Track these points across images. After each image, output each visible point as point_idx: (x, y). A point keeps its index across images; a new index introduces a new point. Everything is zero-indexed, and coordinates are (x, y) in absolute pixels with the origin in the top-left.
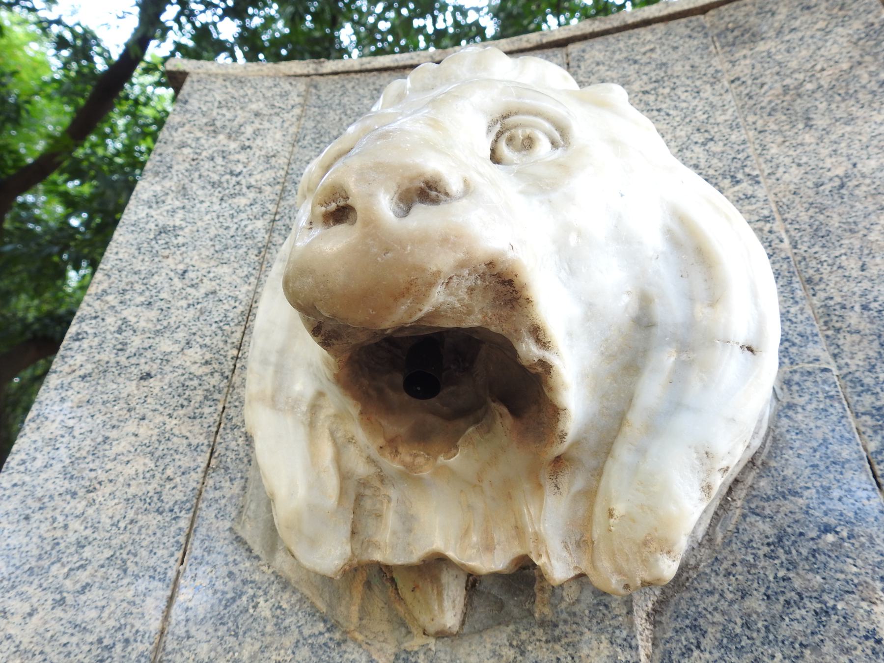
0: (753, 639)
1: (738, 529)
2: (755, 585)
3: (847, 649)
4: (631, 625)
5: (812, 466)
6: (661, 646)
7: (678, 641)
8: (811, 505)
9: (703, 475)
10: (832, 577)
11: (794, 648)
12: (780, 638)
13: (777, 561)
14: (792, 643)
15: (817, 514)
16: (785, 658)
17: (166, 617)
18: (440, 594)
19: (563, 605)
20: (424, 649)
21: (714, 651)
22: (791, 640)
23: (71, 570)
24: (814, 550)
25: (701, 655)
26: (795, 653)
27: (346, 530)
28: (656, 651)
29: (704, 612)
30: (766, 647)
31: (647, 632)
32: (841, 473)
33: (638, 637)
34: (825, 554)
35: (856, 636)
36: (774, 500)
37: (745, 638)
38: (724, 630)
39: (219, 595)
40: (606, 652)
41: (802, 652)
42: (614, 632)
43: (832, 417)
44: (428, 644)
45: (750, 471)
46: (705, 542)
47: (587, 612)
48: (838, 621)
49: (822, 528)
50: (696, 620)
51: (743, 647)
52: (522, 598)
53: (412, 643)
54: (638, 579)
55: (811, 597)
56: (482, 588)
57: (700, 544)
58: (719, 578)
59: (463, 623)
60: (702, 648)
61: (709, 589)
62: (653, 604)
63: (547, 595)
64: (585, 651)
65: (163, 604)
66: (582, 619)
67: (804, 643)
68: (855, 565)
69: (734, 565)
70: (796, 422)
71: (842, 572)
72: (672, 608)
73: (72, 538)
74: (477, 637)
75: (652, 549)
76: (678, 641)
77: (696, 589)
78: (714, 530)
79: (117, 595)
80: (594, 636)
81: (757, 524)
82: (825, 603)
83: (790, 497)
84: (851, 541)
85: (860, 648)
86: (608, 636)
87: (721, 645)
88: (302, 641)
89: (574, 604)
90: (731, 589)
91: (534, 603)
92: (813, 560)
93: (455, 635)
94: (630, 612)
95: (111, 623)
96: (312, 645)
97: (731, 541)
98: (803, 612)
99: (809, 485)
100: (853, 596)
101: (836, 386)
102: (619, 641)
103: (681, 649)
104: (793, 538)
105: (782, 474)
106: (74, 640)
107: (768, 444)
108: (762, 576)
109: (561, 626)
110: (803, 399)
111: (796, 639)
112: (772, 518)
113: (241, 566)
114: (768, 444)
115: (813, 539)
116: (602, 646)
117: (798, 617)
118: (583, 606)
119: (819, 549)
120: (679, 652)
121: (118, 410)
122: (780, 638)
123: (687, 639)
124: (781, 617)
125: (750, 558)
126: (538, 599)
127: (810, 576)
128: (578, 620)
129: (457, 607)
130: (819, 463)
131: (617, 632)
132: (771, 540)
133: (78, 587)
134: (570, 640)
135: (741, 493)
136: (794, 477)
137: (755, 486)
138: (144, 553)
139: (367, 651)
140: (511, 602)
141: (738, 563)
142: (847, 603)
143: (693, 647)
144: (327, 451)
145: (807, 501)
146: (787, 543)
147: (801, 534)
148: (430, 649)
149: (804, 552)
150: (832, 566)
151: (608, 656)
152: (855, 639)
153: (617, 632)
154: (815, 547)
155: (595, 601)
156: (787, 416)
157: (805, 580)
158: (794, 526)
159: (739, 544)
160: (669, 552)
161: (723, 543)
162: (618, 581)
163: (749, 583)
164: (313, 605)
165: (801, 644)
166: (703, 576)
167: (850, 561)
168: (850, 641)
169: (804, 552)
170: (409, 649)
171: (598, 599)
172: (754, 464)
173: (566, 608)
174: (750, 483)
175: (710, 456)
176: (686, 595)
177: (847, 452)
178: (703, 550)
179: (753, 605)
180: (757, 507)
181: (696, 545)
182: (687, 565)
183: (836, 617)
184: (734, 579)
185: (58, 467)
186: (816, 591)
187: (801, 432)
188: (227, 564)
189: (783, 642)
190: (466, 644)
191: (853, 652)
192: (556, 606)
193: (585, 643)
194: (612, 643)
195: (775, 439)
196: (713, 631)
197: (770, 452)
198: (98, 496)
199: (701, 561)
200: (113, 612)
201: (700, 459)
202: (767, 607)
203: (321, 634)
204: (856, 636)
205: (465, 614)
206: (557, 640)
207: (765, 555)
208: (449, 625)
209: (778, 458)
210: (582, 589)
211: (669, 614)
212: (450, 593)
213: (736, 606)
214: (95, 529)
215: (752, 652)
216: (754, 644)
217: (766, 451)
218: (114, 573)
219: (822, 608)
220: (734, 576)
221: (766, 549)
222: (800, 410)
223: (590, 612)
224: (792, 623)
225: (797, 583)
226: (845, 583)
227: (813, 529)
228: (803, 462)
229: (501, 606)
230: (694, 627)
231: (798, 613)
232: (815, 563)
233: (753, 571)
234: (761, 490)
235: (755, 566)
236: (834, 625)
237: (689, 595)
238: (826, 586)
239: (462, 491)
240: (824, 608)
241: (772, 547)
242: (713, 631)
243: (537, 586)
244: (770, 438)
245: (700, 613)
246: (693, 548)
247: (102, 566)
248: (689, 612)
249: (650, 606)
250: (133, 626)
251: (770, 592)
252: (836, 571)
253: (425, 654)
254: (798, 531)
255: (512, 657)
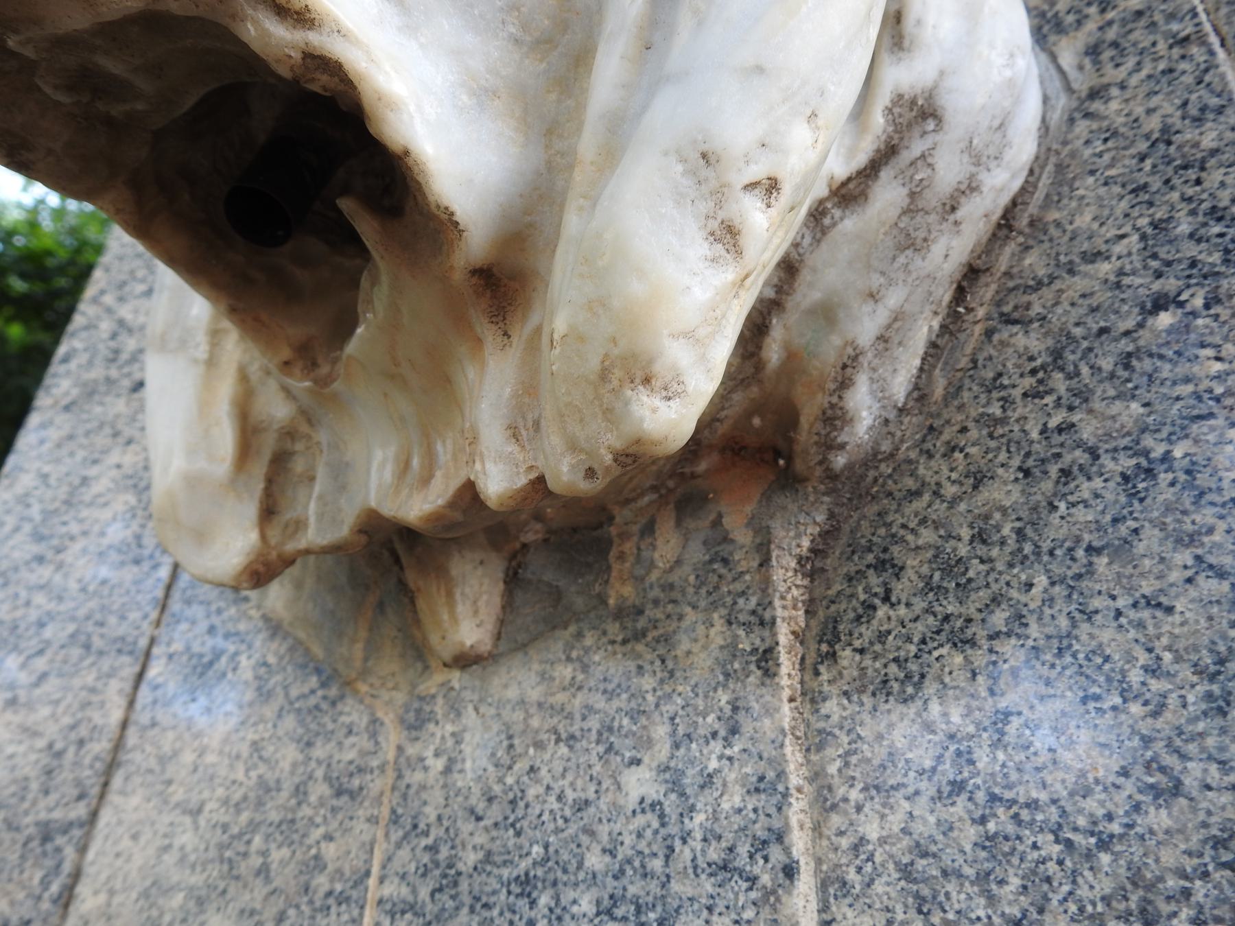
0: (991, 560)
1: (974, 362)
2: (1003, 456)
3: (1191, 536)
4: (766, 585)
5: (1133, 191)
6: (821, 614)
7: (852, 596)
8: (1128, 268)
9: (705, 207)
10: (1166, 397)
11: (1073, 559)
12: (1046, 546)
13: (1049, 400)
14: (1070, 550)
15: (1138, 281)
16: (1053, 584)
17: (131, 703)
18: (450, 594)
19: (654, 576)
20: (444, 690)
21: (915, 600)
22: (1067, 544)
23: (29, 658)
24: (1129, 355)
25: (891, 613)
26: (1076, 569)
27: (250, 509)
28: (813, 623)
29: (902, 532)
30: (1015, 571)
31: (795, 592)
32: (1198, 182)
33: (777, 603)
34: (1151, 355)
35: (1212, 504)
36: (1050, 283)
37: (976, 561)
38: (936, 556)
39: (194, 661)
40: (720, 641)
41: (1091, 564)
42: (735, 603)
43: (1183, 78)
44: (449, 681)
45: (1002, 247)
46: (911, 404)
47: (692, 578)
48: (1172, 484)
49: (1149, 305)
50: (885, 550)
51: (970, 580)
52: (590, 578)
53: (429, 683)
54: (603, 451)
55: (1115, 450)
56: (529, 575)
57: (901, 411)
58: (933, 463)
59: (498, 637)
60: (894, 599)
61: (914, 488)
62: (812, 541)
63: (627, 565)
64: (685, 645)
65: (128, 687)
66: (683, 592)
67: (1096, 544)
68: (1218, 359)
69: (964, 430)
70: (1106, 118)
71: (1187, 380)
72: (844, 540)
73: (33, 615)
74: (520, 655)
75: (615, 383)
76: (852, 596)
77: (890, 494)
78: (930, 376)
79: (77, 682)
80: (701, 617)
81: (1013, 340)
82: (1146, 453)
83: (1084, 268)
84: (1212, 312)
85: (1222, 526)
86: (724, 612)
87: (929, 587)
88: (287, 707)
89: (671, 569)
90: (954, 476)
91: (607, 582)
92: (1126, 374)
93: (486, 659)
94: (765, 562)
95: (67, 720)
96: (299, 711)
97: (960, 388)
98: (1098, 483)
99: (1127, 229)
100: (1212, 422)
101: (1195, 15)
102: (742, 618)
103: (855, 610)
104: (1085, 344)
105: (1070, 228)
106: (21, 749)
107: (1045, 182)
108: (1017, 435)
109: (650, 612)
110: (1122, 68)
111: (1078, 540)
112: (1044, 318)
113: (226, 615)
114: (1045, 182)
115: (1127, 333)
116: (713, 632)
117: (1086, 495)
118: (686, 569)
119: (1138, 349)
120: (852, 615)
121: (101, 440)
122: (1046, 546)
123: (867, 590)
124: (1051, 504)
125: (996, 410)
126: (614, 574)
127: (1117, 406)
128: (676, 595)
129: (483, 611)
130: (1149, 179)
131: (741, 601)
132: (1039, 362)
133: (33, 678)
134: (661, 631)
135: (986, 291)
136: (1095, 226)
137: (1015, 270)
138: (113, 620)
139: (370, 707)
140: (573, 589)
141: (971, 425)
142: (1196, 441)
143: (877, 601)
144: (226, 389)
145: (1119, 263)
146: (1071, 357)
147: (1103, 331)
148: (452, 689)
149: (1107, 364)
150: (1165, 374)
151: (722, 647)
152: (1210, 511)
153: (741, 601)
154: (1131, 348)
155: (707, 557)
156: (1088, 115)
157: (1104, 417)
158: (1089, 320)
159: (975, 388)
160: (647, 381)
161: (945, 398)
162: (573, 466)
163: (990, 456)
164: (307, 651)
165: (1090, 549)
166: (904, 467)
167: (1209, 352)
168: (1198, 518)
169: (1107, 364)
170: (423, 694)
171: (713, 551)
172: (1010, 228)
173: (659, 579)
174: (1003, 269)
175: (713, 159)
176: (871, 510)
177: (1214, 134)
178: (906, 420)
179: (996, 495)
180: (1016, 308)
181: (892, 415)
182: (875, 454)
183: (1170, 476)
184: (961, 456)
185: (27, 528)
186: (1129, 434)
187: (1115, 134)
188: (208, 616)
189: (1051, 553)
190: (503, 670)
191: (1206, 539)
192: (642, 579)
193: (686, 631)
194: (730, 623)
195: (1060, 168)
196: (915, 563)
197: (1048, 196)
198: (68, 557)
199: (902, 441)
200: (69, 706)
201: (691, 172)
202: (1023, 491)
203: (313, 692)
204: (1212, 504)
205: (502, 622)
206: (639, 635)
207: (1025, 395)
208: (468, 643)
209: (1065, 201)
210: (687, 540)
211: (837, 553)
212: (467, 590)
213: (962, 507)
214: (60, 599)
215: (988, 585)
216: (993, 569)
217: (1039, 195)
218: (76, 652)
219: (1138, 466)
220: (961, 451)
221: (1028, 382)
222: (1115, 91)
223: (697, 577)
224: (1073, 510)
225: (1088, 431)
226: (1192, 402)
227: (1129, 313)
228: (1117, 189)
229: (557, 596)
230: (880, 566)
231: (1086, 489)
232: (1128, 380)
233: (1000, 431)
234: (1027, 273)
235: (1003, 421)
236: (1163, 491)
237: (876, 508)
238: (1150, 420)
239: (386, 395)
240: (1144, 463)
241: (1041, 375)
242: (915, 563)
243: (613, 554)
244: (1050, 168)
245: (893, 536)
246: (887, 421)
247: (63, 647)
248: (875, 539)
249: (806, 543)
250: (90, 720)
251: (1030, 462)
252: (1174, 383)
253: (445, 696)
254: (1095, 327)
255: (569, 677)
